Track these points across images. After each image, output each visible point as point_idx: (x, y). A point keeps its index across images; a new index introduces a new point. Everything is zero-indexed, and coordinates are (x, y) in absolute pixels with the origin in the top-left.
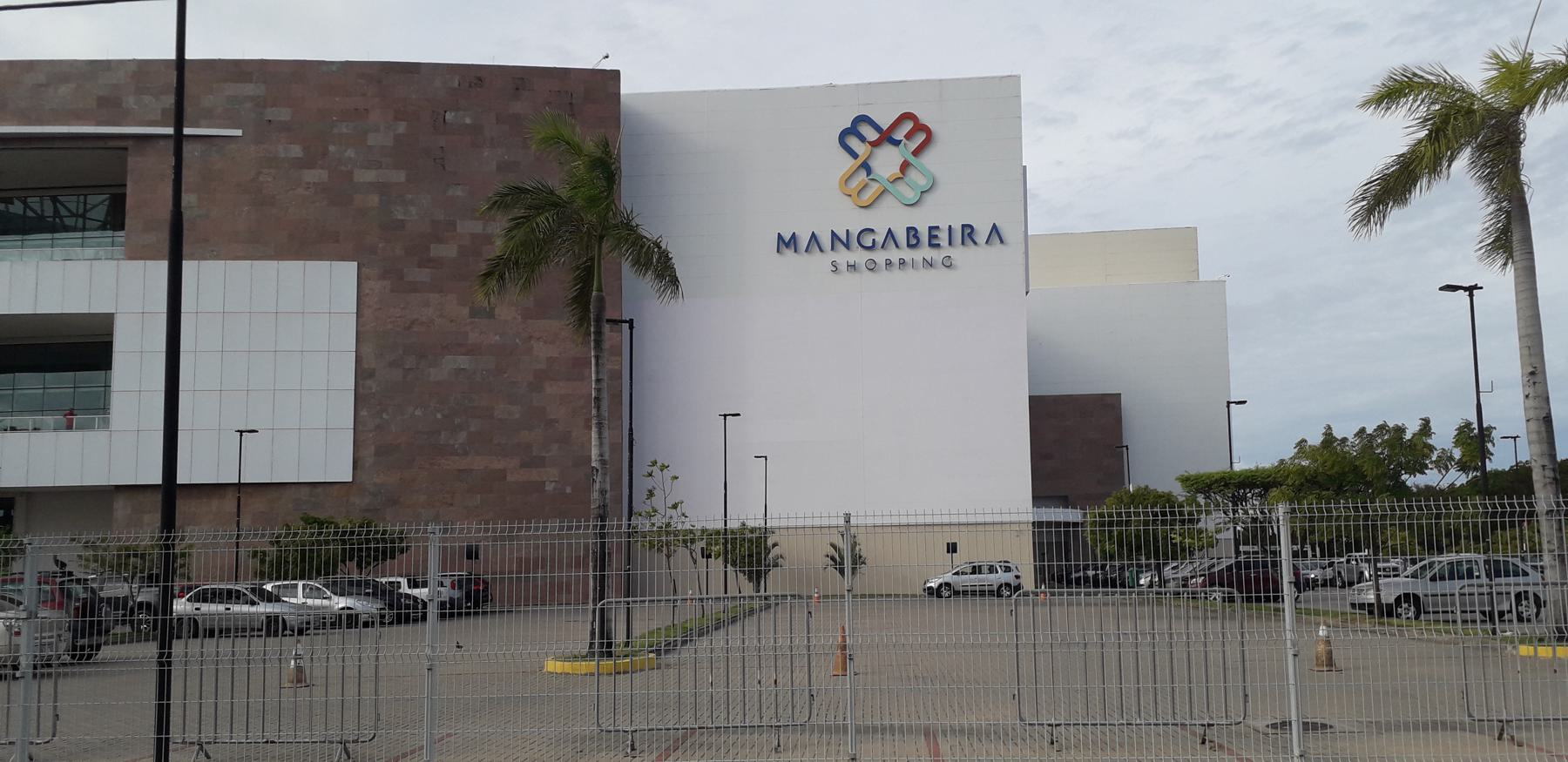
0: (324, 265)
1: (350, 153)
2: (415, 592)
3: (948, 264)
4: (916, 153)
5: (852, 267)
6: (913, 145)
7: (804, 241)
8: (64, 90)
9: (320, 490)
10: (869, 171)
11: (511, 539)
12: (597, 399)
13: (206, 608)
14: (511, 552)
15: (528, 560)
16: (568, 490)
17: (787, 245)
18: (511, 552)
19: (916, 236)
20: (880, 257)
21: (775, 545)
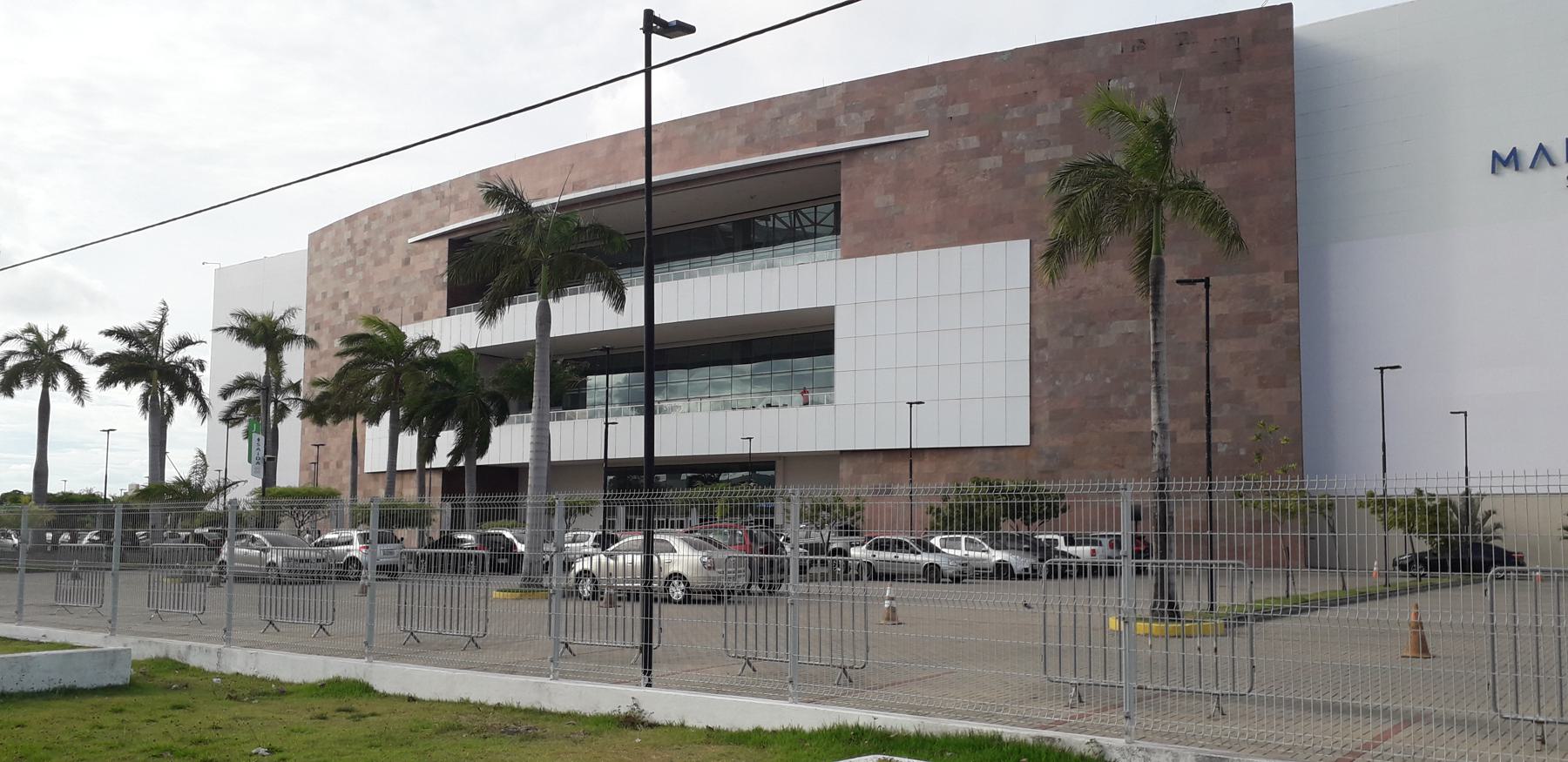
0: (890, 258)
1: (1021, 136)
2: (1071, 550)
7: (1528, 154)
9: (1002, 453)
12: (1155, 363)
16: (1242, 452)
17: (1506, 163)
18: (1188, 514)
21: (1488, 514)
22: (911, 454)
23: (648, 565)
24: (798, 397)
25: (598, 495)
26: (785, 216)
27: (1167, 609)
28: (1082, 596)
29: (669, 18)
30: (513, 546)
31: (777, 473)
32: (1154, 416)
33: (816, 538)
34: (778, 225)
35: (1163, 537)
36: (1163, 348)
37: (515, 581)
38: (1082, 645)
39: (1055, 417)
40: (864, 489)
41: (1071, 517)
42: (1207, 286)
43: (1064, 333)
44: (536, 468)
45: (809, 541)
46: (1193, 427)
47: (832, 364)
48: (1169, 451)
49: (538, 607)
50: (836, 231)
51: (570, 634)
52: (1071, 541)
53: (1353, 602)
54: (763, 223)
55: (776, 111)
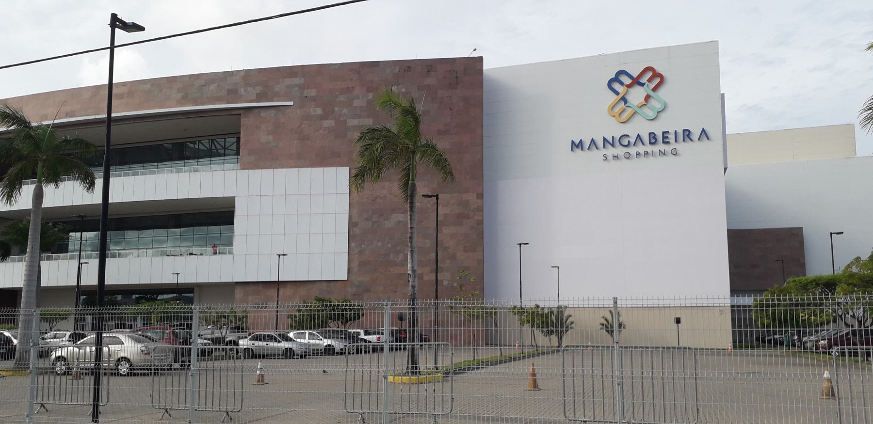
1: (345, 111)
3: (675, 153)
4: (654, 89)
5: (616, 157)
6: (652, 85)
7: (587, 144)
8: (212, 87)
9: (332, 284)
10: (626, 102)
11: (426, 308)
13: (257, 343)
14: (426, 317)
15: (334, 320)
16: (455, 285)
17: (577, 147)
18: (426, 317)
19: (654, 138)
20: (633, 150)
22: (279, 284)
23: (99, 352)
24: (210, 249)
25: (72, 309)
26: (206, 142)
27: (413, 368)
28: (367, 365)
29: (128, 20)
30: (10, 341)
31: (195, 295)
32: (409, 265)
33: (217, 334)
34: (201, 147)
35: (414, 331)
36: (415, 230)
37: (10, 364)
38: (366, 391)
39: (362, 264)
40: (249, 306)
41: (366, 319)
42: (437, 199)
43: (367, 219)
44: (27, 291)
45: (213, 336)
46: (431, 272)
47: (232, 231)
48: (416, 284)
49: (25, 382)
50: (238, 153)
51: (45, 398)
52: (366, 333)
53: (505, 362)
54: (192, 145)
55: (202, 82)
